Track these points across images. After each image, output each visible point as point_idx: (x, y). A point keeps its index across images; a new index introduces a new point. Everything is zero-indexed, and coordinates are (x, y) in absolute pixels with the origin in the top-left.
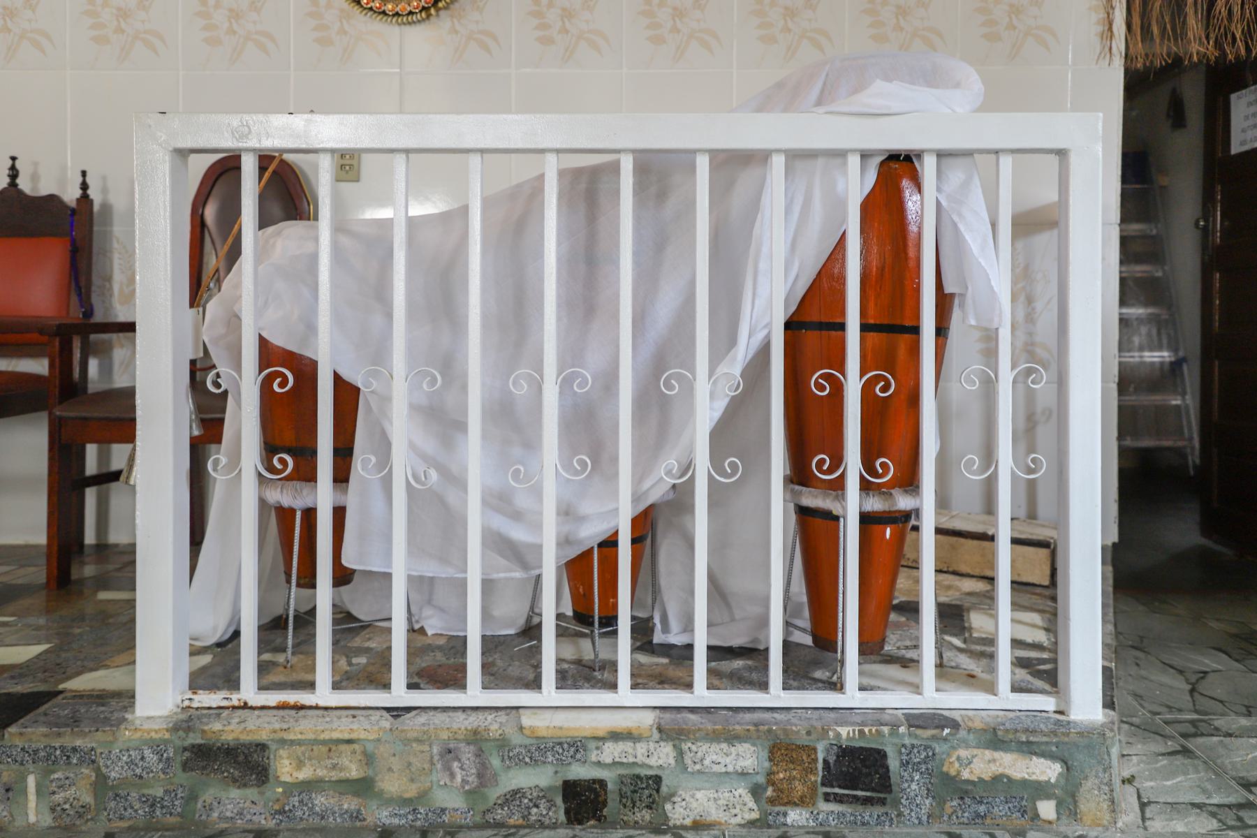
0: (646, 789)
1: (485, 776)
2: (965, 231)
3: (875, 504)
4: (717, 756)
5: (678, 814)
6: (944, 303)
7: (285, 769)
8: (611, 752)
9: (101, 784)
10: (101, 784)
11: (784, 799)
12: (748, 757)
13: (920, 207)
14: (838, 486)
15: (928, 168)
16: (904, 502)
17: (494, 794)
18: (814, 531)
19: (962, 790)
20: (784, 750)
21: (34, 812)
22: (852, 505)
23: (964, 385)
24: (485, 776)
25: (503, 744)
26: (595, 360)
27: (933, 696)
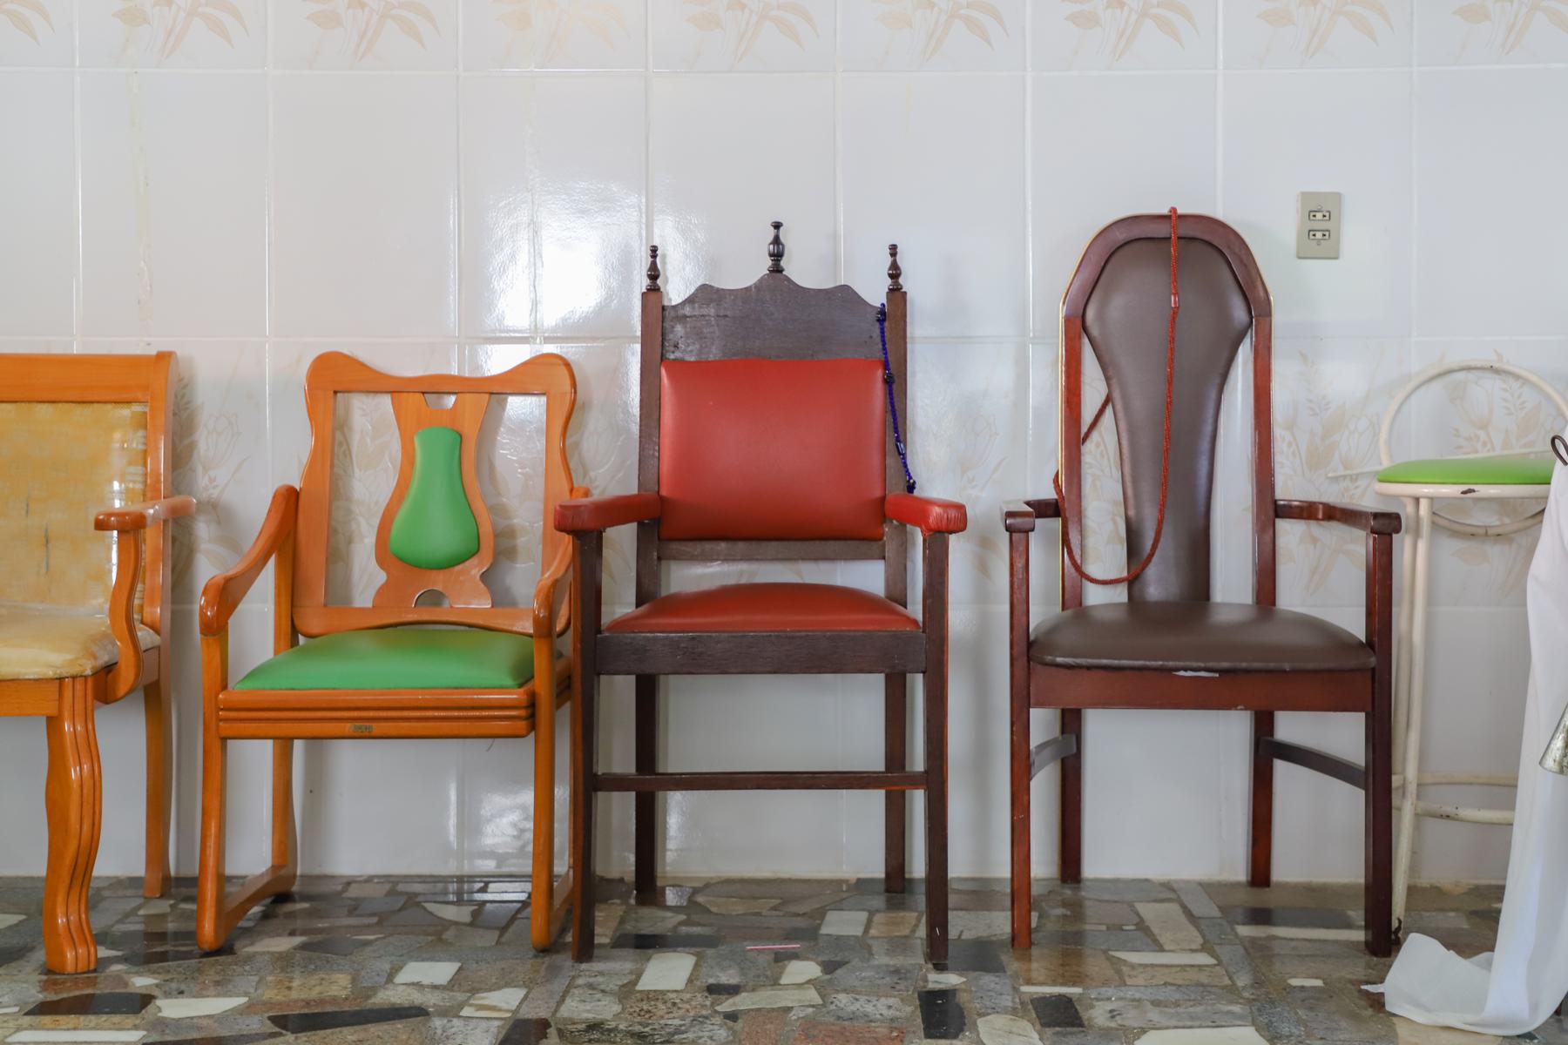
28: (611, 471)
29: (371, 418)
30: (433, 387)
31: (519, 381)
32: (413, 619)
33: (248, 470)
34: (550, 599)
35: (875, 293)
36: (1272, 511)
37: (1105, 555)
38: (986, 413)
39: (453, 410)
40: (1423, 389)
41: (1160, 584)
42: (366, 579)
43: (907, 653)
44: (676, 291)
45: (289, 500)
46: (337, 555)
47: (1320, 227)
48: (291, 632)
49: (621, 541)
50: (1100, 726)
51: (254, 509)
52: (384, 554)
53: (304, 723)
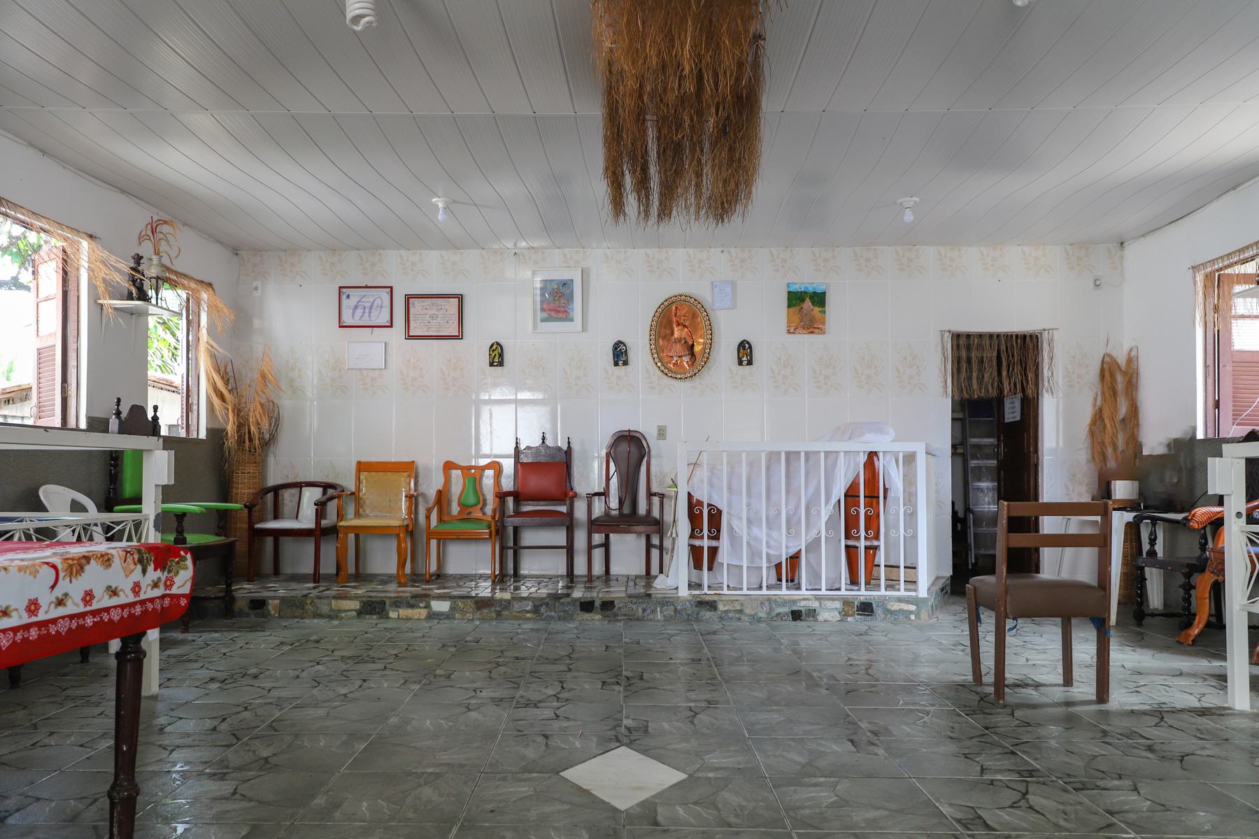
0: (812, 613)
1: (771, 609)
2: (892, 474)
3: (868, 543)
4: (829, 604)
5: (820, 618)
6: (886, 490)
7: (721, 607)
8: (803, 603)
9: (676, 610)
10: (676, 610)
11: (847, 615)
12: (838, 605)
13: (880, 464)
14: (858, 538)
15: (881, 455)
16: (875, 543)
17: (774, 614)
18: (851, 552)
19: (892, 613)
20: (847, 602)
21: (659, 616)
22: (862, 544)
23: (892, 510)
24: (771, 609)
25: (776, 601)
26: (791, 506)
27: (883, 592)
28: (507, 484)
29: (456, 473)
30: (470, 468)
31: (488, 467)
32: (465, 516)
33: (432, 485)
34: (494, 511)
35: (565, 448)
36: (650, 495)
37: (614, 504)
38: (592, 473)
39: (473, 475)
40: (494, 422)
41: (626, 510)
42: (455, 509)
43: (569, 523)
44: (522, 447)
45: (439, 493)
46: (449, 504)
47: (662, 433)
48: (440, 520)
49: (510, 500)
50: (613, 537)
51: (432, 494)
52: (460, 504)
53: (444, 538)
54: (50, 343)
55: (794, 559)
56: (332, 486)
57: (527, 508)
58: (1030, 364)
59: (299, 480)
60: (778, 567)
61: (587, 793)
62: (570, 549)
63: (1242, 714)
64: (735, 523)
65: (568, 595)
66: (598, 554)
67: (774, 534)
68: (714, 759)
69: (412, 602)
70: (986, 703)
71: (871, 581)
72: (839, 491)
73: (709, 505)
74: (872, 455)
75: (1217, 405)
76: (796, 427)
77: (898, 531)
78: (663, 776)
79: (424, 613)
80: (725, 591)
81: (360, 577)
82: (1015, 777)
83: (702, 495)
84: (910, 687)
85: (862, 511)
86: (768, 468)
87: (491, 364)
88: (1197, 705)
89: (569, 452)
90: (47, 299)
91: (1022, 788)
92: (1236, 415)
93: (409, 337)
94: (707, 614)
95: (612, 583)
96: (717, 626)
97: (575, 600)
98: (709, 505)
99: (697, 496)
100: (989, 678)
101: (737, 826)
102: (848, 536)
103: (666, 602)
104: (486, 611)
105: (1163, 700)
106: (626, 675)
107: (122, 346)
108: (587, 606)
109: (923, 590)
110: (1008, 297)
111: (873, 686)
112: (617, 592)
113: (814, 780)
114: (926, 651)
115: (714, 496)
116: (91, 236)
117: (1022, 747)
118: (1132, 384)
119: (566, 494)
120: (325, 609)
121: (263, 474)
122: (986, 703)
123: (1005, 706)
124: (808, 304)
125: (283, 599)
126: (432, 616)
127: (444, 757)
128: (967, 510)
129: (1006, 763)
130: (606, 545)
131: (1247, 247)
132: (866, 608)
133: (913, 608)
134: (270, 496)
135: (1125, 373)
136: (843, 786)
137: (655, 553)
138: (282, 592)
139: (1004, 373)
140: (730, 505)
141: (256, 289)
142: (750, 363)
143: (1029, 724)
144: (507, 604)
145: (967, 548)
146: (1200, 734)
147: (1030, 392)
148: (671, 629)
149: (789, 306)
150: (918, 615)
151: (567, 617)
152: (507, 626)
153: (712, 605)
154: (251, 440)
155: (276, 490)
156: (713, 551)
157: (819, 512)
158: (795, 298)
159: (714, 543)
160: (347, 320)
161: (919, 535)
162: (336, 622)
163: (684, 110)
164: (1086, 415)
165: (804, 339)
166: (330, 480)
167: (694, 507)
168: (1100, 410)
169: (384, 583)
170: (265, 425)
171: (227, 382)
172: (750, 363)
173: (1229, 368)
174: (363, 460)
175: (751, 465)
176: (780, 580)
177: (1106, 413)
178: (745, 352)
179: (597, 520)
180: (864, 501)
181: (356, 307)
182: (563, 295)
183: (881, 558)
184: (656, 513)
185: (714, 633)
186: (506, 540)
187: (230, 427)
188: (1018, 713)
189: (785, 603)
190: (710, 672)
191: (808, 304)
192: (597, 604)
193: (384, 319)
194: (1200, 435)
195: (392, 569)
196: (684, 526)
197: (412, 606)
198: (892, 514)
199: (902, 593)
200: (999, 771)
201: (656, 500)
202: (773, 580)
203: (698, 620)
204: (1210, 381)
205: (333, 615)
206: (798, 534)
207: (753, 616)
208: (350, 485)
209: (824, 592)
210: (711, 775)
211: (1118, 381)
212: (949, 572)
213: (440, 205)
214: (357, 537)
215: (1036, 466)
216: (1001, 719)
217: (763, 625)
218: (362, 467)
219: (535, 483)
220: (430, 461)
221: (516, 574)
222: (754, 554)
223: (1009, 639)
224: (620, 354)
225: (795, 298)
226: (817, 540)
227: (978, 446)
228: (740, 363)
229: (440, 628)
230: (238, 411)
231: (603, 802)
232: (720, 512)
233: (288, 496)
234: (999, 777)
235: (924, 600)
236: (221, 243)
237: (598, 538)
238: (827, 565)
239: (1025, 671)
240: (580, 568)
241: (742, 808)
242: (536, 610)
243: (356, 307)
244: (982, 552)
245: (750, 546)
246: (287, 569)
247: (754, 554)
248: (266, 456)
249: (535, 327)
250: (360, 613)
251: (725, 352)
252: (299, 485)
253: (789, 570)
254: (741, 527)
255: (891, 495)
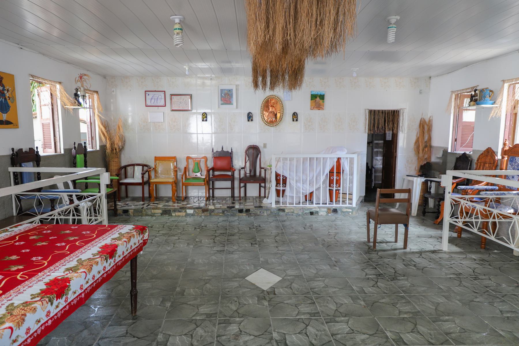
0: (317, 212)
1: (303, 211)
2: (346, 166)
4: (323, 210)
5: (320, 214)
6: (343, 171)
7: (286, 211)
11: (329, 213)
12: (326, 210)
13: (342, 161)
16: (339, 188)
18: (331, 191)
20: (329, 209)
21: (265, 214)
22: (335, 189)
27: (341, 205)
28: (211, 165)
31: (203, 158)
33: (182, 165)
36: (261, 168)
37: (248, 172)
38: (239, 162)
41: (252, 174)
43: (232, 179)
45: (185, 168)
47: (265, 146)
49: (211, 171)
54: (48, 121)
55: (311, 194)
56: (146, 166)
57: (217, 173)
58: (396, 119)
59: (133, 163)
60: (306, 196)
61: (254, 285)
62: (233, 188)
63: (445, 252)
64: (292, 182)
65: (234, 207)
66: (242, 190)
67: (305, 185)
68: (289, 272)
69: (180, 210)
70: (371, 247)
71: (337, 201)
72: (327, 171)
73: (283, 176)
74: (339, 159)
75: (456, 140)
76: (314, 146)
77: (347, 184)
78: (275, 279)
79: (184, 214)
80: (288, 205)
81: (158, 199)
82: (375, 276)
83: (280, 172)
84: (349, 243)
85: (335, 178)
86: (303, 162)
87: (203, 121)
88: (433, 249)
89: (231, 153)
90: (45, 105)
91: (376, 280)
92: (462, 144)
93: (173, 110)
94: (281, 213)
95: (248, 201)
96: (285, 218)
97: (237, 209)
98: (283, 176)
99: (278, 172)
100: (372, 240)
101: (297, 294)
102: (330, 186)
103: (267, 209)
104: (206, 213)
105: (423, 247)
106: (255, 238)
107: (72, 121)
108: (241, 211)
109: (354, 205)
110: (390, 96)
111: (336, 243)
112: (249, 205)
113: (318, 279)
114: (354, 228)
115: (285, 172)
116: (60, 83)
117: (378, 266)
118: (430, 130)
119: (230, 168)
120: (149, 213)
121: (120, 162)
122: (371, 247)
123: (376, 251)
124: (318, 99)
125: (134, 210)
126: (187, 215)
127: (209, 273)
128: (372, 167)
129: (373, 272)
130: (245, 187)
131: (468, 89)
132: (335, 211)
133: (351, 210)
134: (123, 170)
135: (428, 125)
136: (327, 281)
137: (262, 189)
138: (133, 207)
139: (386, 125)
140: (290, 174)
141: (113, 91)
142: (297, 120)
143: (382, 258)
144: (212, 211)
145: (371, 181)
146: (431, 260)
147: (395, 131)
148: (271, 219)
149: (311, 100)
150: (352, 213)
151: (233, 215)
152: (214, 219)
153: (283, 210)
154: (116, 149)
155: (125, 167)
156: (284, 191)
157: (320, 178)
158: (314, 97)
159: (284, 188)
160: (149, 103)
161: (355, 184)
162: (154, 218)
163: (279, 66)
164: (414, 139)
165: (316, 112)
166: (145, 163)
167: (277, 175)
168: (418, 138)
169: (167, 201)
170: (120, 144)
171: (105, 128)
172: (297, 120)
173: (461, 128)
174: (157, 156)
175: (297, 161)
176: (306, 200)
177: (420, 140)
178: (295, 116)
179: (243, 178)
180: (336, 172)
181: (152, 99)
182: (229, 95)
183: (341, 192)
184: (263, 175)
185: (284, 221)
186: (209, 182)
187: (108, 146)
188: (380, 253)
189: (308, 209)
190: (283, 237)
191: (318, 99)
192: (244, 210)
193: (162, 103)
194: (449, 151)
195: (170, 194)
196: (274, 182)
197: (180, 212)
198: (345, 177)
199: (347, 205)
200: (371, 275)
201: (263, 170)
202: (304, 200)
203: (279, 215)
204: (454, 132)
205: (152, 215)
206: (313, 185)
207: (297, 214)
208: (152, 165)
209: (321, 205)
210: (289, 278)
211: (425, 127)
212: (364, 194)
213: (187, 69)
214: (156, 185)
215: (396, 157)
216: (374, 256)
217: (301, 217)
218: (157, 159)
219: (221, 163)
220: (181, 156)
221: (213, 196)
222: (298, 192)
223: (378, 230)
224: (250, 117)
225: (314, 97)
226: (319, 188)
227: (377, 144)
228: (293, 121)
229: (189, 220)
230: (110, 139)
231: (260, 288)
232: (286, 178)
233: (129, 169)
234: (370, 277)
235: (354, 208)
236: (99, 75)
237: (242, 185)
238: (323, 195)
239: (383, 237)
240: (236, 194)
241: (299, 289)
242: (223, 212)
243: (152, 99)
244: (377, 182)
245: (296, 190)
246: (130, 195)
247: (298, 192)
248: (121, 154)
249: (219, 107)
250: (162, 214)
251: (288, 117)
252: (133, 165)
253: (309, 197)
254: (294, 183)
255: (345, 172)
